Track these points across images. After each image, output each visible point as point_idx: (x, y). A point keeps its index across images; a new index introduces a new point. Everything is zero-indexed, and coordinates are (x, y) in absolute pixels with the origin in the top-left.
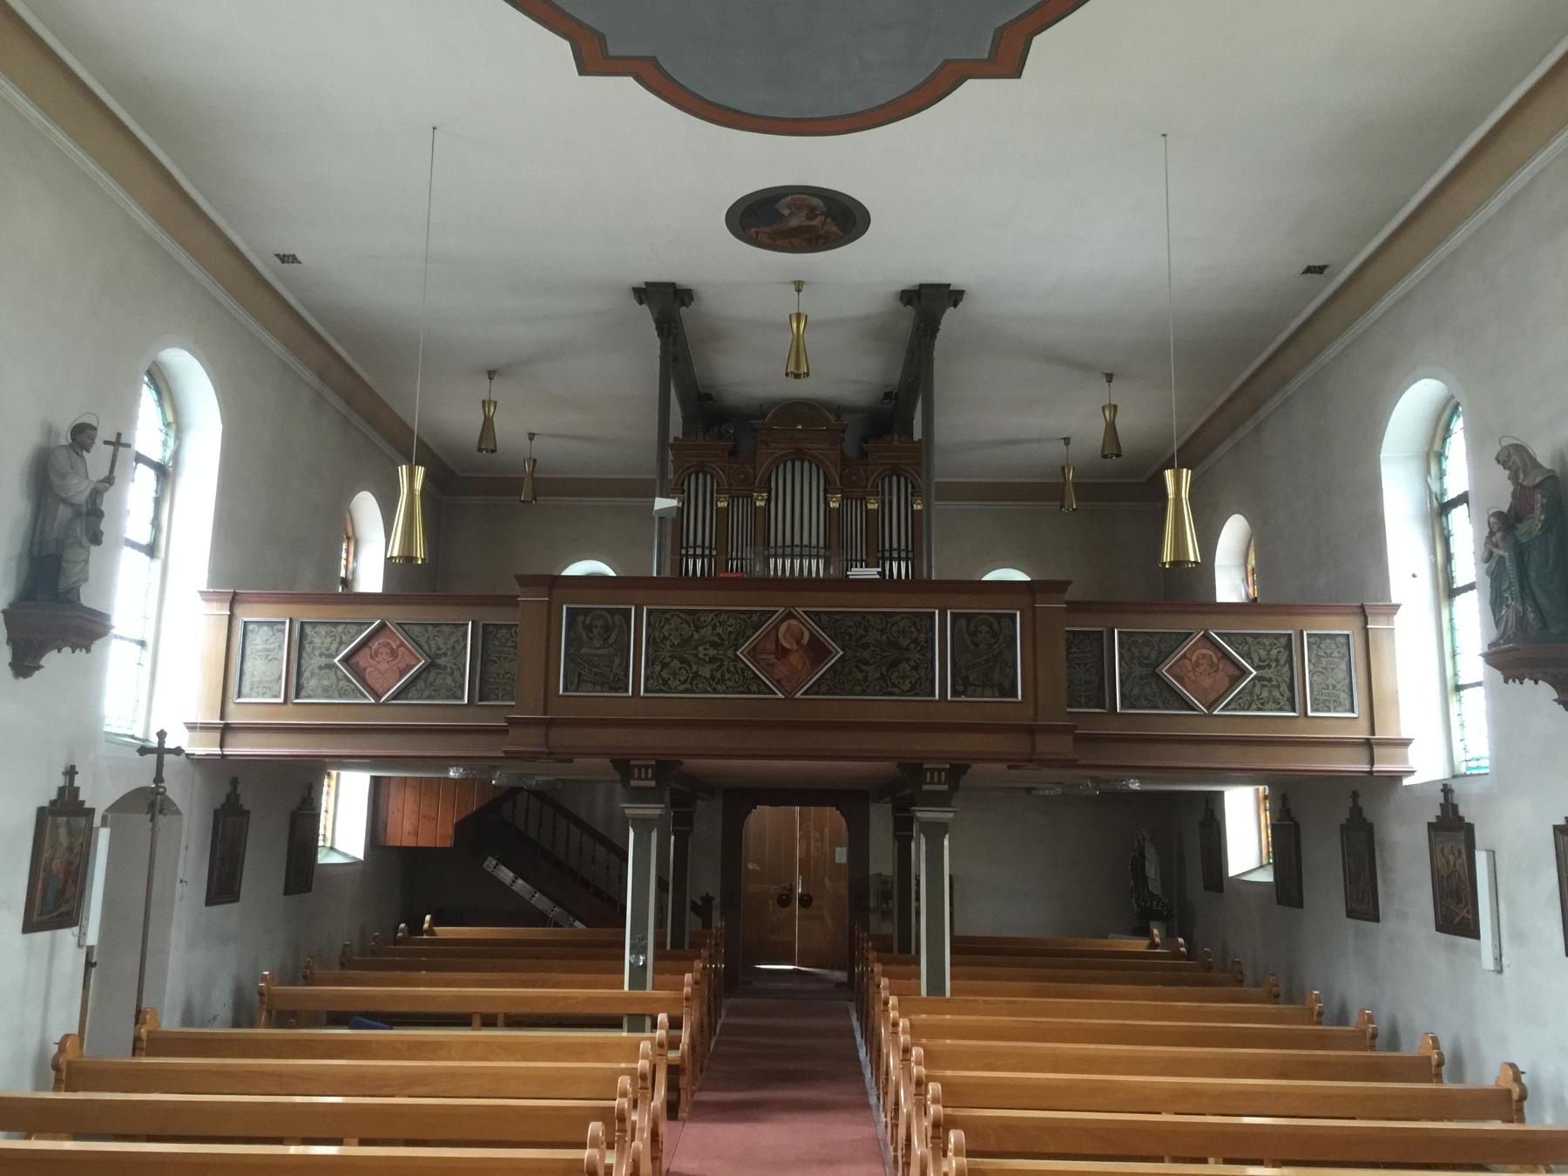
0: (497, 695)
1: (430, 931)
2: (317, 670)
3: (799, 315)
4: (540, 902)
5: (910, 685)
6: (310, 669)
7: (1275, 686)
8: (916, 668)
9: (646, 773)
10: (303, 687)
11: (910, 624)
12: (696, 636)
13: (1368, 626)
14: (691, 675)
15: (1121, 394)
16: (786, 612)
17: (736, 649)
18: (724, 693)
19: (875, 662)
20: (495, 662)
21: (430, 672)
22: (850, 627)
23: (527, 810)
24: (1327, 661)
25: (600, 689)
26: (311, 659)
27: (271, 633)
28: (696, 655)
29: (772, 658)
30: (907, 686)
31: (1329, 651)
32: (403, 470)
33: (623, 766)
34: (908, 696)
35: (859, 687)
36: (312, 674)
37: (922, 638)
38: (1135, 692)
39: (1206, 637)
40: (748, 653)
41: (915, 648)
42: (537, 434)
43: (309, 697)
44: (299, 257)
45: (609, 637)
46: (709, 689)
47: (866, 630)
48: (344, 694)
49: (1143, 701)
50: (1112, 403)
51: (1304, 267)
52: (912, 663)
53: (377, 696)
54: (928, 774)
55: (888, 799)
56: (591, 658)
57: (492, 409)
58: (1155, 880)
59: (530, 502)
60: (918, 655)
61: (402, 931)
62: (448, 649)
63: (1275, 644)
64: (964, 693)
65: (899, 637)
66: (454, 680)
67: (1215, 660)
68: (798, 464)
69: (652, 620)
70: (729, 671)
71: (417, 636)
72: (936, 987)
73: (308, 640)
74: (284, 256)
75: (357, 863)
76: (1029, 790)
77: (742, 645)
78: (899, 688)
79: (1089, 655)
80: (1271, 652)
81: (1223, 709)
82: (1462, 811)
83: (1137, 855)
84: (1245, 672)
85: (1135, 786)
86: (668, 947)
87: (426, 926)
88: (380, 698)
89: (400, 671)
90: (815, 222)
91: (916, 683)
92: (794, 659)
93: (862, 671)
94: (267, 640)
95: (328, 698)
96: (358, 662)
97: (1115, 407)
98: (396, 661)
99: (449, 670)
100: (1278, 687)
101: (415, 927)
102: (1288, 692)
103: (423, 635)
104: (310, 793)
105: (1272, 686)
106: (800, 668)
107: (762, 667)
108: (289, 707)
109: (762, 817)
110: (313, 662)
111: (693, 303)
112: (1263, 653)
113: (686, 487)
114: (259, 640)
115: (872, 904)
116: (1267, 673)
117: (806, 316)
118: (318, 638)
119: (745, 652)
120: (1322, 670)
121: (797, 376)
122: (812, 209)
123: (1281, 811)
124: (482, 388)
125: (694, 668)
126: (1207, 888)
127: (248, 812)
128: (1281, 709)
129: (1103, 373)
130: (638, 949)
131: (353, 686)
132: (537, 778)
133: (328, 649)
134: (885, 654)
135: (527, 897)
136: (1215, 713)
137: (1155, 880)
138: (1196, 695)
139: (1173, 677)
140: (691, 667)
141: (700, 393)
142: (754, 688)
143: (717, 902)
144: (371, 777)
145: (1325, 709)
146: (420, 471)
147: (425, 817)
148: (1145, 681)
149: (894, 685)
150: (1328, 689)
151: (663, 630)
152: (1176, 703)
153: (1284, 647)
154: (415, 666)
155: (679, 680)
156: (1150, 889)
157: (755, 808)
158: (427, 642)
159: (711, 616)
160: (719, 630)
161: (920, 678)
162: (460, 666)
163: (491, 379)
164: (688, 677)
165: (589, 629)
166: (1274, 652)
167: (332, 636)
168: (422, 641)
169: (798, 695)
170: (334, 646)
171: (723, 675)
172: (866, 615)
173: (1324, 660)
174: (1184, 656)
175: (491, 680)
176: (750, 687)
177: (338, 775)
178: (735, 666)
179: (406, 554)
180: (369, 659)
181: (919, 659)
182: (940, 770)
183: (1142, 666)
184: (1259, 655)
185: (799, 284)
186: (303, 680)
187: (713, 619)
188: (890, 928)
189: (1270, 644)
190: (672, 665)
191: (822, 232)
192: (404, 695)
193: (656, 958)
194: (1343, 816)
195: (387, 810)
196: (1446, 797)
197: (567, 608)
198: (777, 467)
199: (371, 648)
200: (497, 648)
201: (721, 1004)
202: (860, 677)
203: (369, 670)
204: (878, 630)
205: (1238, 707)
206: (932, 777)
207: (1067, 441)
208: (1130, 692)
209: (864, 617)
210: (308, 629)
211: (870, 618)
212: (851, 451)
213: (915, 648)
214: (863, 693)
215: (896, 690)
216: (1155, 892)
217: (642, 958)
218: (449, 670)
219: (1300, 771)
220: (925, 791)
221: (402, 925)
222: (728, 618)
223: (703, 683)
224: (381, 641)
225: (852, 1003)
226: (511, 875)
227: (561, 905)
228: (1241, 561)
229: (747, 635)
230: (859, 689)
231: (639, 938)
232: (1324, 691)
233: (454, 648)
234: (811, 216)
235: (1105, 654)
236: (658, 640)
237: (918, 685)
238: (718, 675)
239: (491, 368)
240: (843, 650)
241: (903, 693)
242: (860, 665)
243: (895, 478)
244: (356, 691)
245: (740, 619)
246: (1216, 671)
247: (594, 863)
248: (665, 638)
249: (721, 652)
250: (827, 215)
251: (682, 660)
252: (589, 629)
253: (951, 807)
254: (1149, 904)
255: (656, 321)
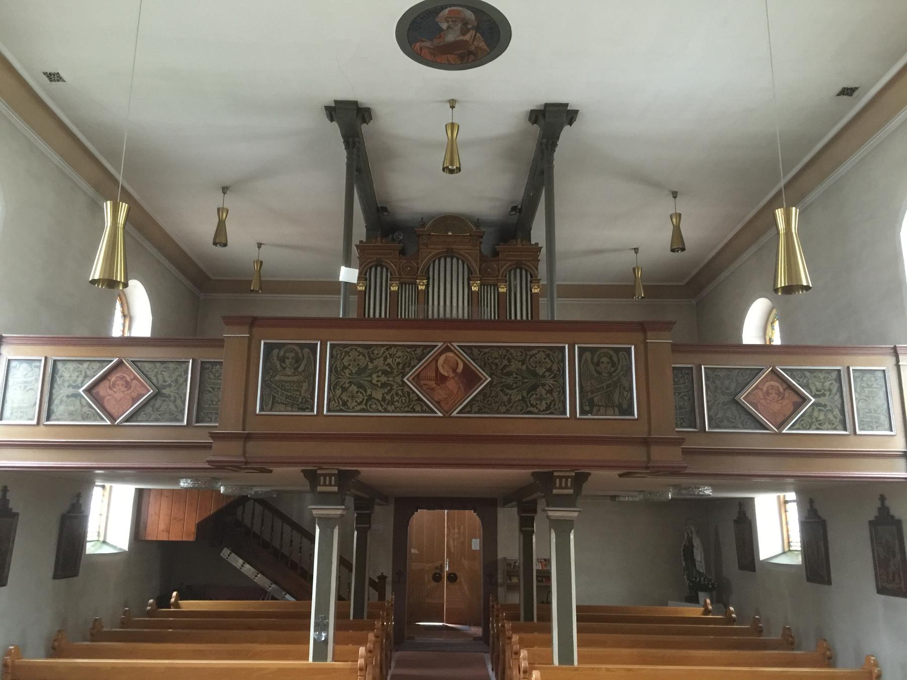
0: (211, 418)
1: (176, 605)
2: (65, 398)
3: (453, 124)
4: (261, 580)
5: (546, 406)
6: (60, 397)
7: (830, 410)
8: (550, 392)
9: (330, 481)
10: (53, 412)
11: (545, 356)
12: (371, 366)
13: (900, 364)
14: (366, 398)
15: (683, 206)
16: (444, 346)
17: (403, 376)
18: (393, 412)
19: (517, 387)
20: (210, 392)
21: (157, 399)
22: (496, 358)
23: (253, 514)
24: (869, 391)
25: (290, 409)
26: (60, 389)
27: (30, 369)
28: (371, 381)
29: (433, 384)
30: (543, 406)
31: (870, 383)
32: (108, 206)
33: (312, 477)
34: (544, 414)
35: (504, 407)
36: (61, 401)
37: (555, 367)
38: (719, 415)
39: (774, 372)
40: (413, 379)
41: (550, 375)
42: (263, 244)
43: (58, 420)
44: (62, 75)
45: (298, 367)
46: (380, 409)
47: (509, 360)
48: (87, 417)
49: (726, 422)
50: (678, 212)
51: (838, 89)
52: (547, 388)
53: (112, 418)
54: (558, 480)
55: (515, 503)
56: (284, 383)
57: (224, 215)
58: (700, 562)
59: (257, 292)
60: (551, 381)
61: (151, 605)
62: (172, 382)
63: (828, 378)
64: (591, 412)
65: (536, 367)
66: (176, 406)
67: (781, 390)
68: (448, 260)
69: (334, 353)
70: (397, 394)
71: (148, 372)
72: (565, 656)
73: (59, 374)
74: (50, 74)
75: (122, 553)
76: (613, 497)
77: (408, 373)
78: (537, 408)
79: (682, 386)
80: (824, 384)
81: (789, 429)
82: (892, 512)
83: (687, 544)
84: (804, 400)
85: (708, 492)
86: (351, 618)
87: (173, 600)
88: (116, 421)
89: (133, 399)
90: (467, 37)
91: (551, 403)
92: (452, 384)
93: (506, 395)
94: (26, 374)
95: (72, 420)
96: (98, 393)
97: (680, 215)
98: (129, 392)
99: (173, 398)
100: (831, 411)
101: (163, 601)
102: (839, 415)
103: (153, 371)
104: (78, 500)
105: (827, 410)
106: (455, 391)
107: (425, 391)
108: (41, 428)
109: (422, 518)
110: (61, 392)
111: (371, 121)
112: (818, 385)
113: (368, 276)
114: (19, 373)
115: (500, 580)
116: (822, 400)
117: (458, 126)
118: (67, 373)
119: (410, 379)
120: (864, 397)
121: (452, 172)
122: (465, 23)
123: (809, 511)
124: (218, 200)
125: (369, 392)
126: (742, 567)
127: (17, 515)
128: (835, 429)
129: (670, 191)
130: (321, 626)
131: (94, 411)
132: (256, 489)
133: (75, 382)
134: (526, 380)
135: (252, 577)
136: (784, 431)
137: (700, 562)
138: (768, 418)
139: (748, 403)
140: (366, 391)
141: (378, 208)
142: (418, 408)
143: (389, 579)
144: (136, 489)
145: (869, 428)
146: (124, 208)
147: (175, 518)
148: (727, 406)
149: (532, 406)
150: (871, 412)
151: (343, 361)
152: (752, 425)
153: (835, 380)
154: (144, 395)
155: (356, 401)
156: (697, 568)
157: (417, 511)
158: (156, 376)
159: (383, 349)
160: (389, 361)
161: (554, 400)
162: (182, 395)
163: (224, 193)
164: (363, 399)
165: (282, 360)
166: (827, 384)
167: (78, 372)
168: (151, 375)
169: (454, 414)
170: (80, 380)
171: (392, 397)
172: (509, 349)
173: (867, 390)
174: (757, 387)
175: (206, 406)
176: (415, 407)
177: (111, 487)
178: (402, 390)
179: (106, 277)
180: (108, 389)
181: (553, 384)
182: (567, 478)
183: (724, 395)
184: (815, 385)
185: (453, 102)
186: (54, 407)
187: (384, 352)
188: (515, 598)
189: (824, 378)
190: (350, 389)
191: (472, 48)
192: (135, 419)
193: (337, 628)
194: (871, 513)
195: (148, 514)
196: (741, 508)
197: (265, 343)
198: (434, 262)
199: (110, 381)
200: (212, 381)
201: (391, 656)
202: (505, 399)
203: (108, 398)
204: (519, 361)
205: (801, 427)
206: (561, 483)
207: (636, 250)
208: (715, 416)
209: (507, 351)
210: (60, 366)
211: (512, 351)
212: (486, 248)
213: (550, 375)
214: (507, 412)
215: (535, 410)
216: (701, 571)
217: (323, 634)
218: (173, 398)
219: (875, 478)
220: (555, 495)
221: (151, 601)
222: (397, 351)
223: (376, 404)
224: (118, 375)
225: (488, 654)
226: (241, 561)
227: (275, 583)
228: (761, 334)
229: (412, 365)
230: (503, 409)
231: (322, 617)
232: (867, 414)
233: (176, 381)
234: (464, 32)
235: (695, 386)
236: (339, 369)
237: (552, 406)
238: (388, 397)
239: (225, 185)
240: (490, 376)
241: (540, 412)
242: (505, 389)
243: (518, 270)
244: (96, 415)
245: (407, 352)
246: (783, 398)
247: (300, 552)
248: (345, 368)
249: (391, 379)
250: (477, 29)
251: (360, 386)
252: (282, 360)
253: (575, 506)
254: (698, 580)
255: (344, 136)
